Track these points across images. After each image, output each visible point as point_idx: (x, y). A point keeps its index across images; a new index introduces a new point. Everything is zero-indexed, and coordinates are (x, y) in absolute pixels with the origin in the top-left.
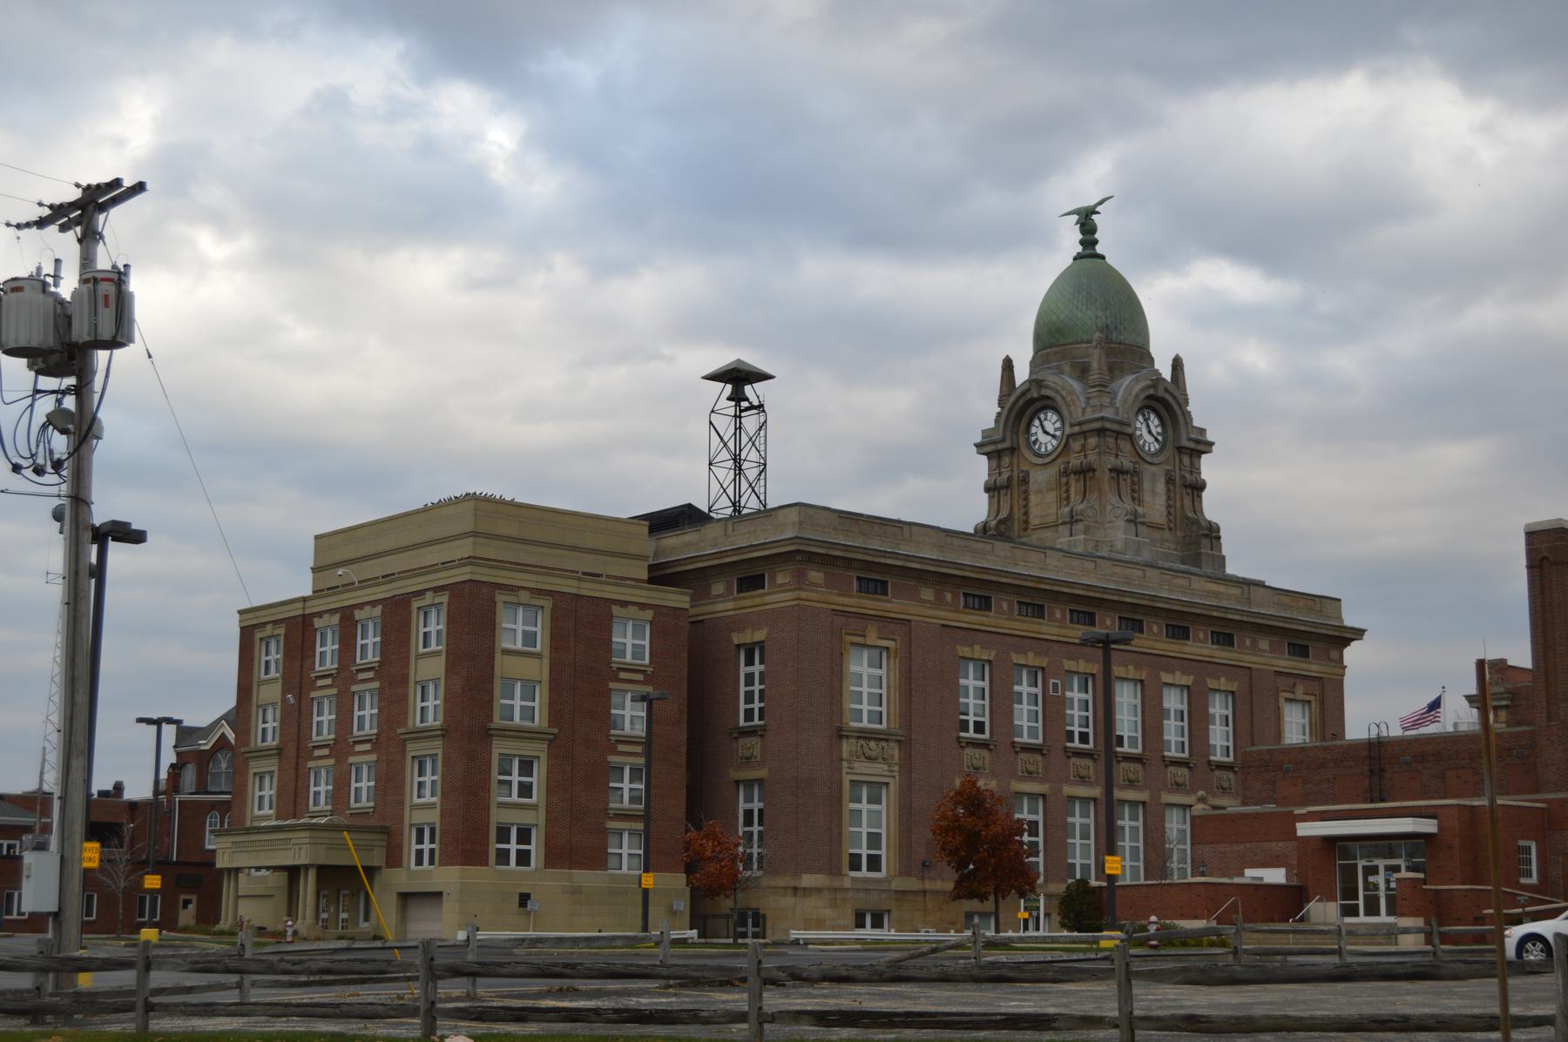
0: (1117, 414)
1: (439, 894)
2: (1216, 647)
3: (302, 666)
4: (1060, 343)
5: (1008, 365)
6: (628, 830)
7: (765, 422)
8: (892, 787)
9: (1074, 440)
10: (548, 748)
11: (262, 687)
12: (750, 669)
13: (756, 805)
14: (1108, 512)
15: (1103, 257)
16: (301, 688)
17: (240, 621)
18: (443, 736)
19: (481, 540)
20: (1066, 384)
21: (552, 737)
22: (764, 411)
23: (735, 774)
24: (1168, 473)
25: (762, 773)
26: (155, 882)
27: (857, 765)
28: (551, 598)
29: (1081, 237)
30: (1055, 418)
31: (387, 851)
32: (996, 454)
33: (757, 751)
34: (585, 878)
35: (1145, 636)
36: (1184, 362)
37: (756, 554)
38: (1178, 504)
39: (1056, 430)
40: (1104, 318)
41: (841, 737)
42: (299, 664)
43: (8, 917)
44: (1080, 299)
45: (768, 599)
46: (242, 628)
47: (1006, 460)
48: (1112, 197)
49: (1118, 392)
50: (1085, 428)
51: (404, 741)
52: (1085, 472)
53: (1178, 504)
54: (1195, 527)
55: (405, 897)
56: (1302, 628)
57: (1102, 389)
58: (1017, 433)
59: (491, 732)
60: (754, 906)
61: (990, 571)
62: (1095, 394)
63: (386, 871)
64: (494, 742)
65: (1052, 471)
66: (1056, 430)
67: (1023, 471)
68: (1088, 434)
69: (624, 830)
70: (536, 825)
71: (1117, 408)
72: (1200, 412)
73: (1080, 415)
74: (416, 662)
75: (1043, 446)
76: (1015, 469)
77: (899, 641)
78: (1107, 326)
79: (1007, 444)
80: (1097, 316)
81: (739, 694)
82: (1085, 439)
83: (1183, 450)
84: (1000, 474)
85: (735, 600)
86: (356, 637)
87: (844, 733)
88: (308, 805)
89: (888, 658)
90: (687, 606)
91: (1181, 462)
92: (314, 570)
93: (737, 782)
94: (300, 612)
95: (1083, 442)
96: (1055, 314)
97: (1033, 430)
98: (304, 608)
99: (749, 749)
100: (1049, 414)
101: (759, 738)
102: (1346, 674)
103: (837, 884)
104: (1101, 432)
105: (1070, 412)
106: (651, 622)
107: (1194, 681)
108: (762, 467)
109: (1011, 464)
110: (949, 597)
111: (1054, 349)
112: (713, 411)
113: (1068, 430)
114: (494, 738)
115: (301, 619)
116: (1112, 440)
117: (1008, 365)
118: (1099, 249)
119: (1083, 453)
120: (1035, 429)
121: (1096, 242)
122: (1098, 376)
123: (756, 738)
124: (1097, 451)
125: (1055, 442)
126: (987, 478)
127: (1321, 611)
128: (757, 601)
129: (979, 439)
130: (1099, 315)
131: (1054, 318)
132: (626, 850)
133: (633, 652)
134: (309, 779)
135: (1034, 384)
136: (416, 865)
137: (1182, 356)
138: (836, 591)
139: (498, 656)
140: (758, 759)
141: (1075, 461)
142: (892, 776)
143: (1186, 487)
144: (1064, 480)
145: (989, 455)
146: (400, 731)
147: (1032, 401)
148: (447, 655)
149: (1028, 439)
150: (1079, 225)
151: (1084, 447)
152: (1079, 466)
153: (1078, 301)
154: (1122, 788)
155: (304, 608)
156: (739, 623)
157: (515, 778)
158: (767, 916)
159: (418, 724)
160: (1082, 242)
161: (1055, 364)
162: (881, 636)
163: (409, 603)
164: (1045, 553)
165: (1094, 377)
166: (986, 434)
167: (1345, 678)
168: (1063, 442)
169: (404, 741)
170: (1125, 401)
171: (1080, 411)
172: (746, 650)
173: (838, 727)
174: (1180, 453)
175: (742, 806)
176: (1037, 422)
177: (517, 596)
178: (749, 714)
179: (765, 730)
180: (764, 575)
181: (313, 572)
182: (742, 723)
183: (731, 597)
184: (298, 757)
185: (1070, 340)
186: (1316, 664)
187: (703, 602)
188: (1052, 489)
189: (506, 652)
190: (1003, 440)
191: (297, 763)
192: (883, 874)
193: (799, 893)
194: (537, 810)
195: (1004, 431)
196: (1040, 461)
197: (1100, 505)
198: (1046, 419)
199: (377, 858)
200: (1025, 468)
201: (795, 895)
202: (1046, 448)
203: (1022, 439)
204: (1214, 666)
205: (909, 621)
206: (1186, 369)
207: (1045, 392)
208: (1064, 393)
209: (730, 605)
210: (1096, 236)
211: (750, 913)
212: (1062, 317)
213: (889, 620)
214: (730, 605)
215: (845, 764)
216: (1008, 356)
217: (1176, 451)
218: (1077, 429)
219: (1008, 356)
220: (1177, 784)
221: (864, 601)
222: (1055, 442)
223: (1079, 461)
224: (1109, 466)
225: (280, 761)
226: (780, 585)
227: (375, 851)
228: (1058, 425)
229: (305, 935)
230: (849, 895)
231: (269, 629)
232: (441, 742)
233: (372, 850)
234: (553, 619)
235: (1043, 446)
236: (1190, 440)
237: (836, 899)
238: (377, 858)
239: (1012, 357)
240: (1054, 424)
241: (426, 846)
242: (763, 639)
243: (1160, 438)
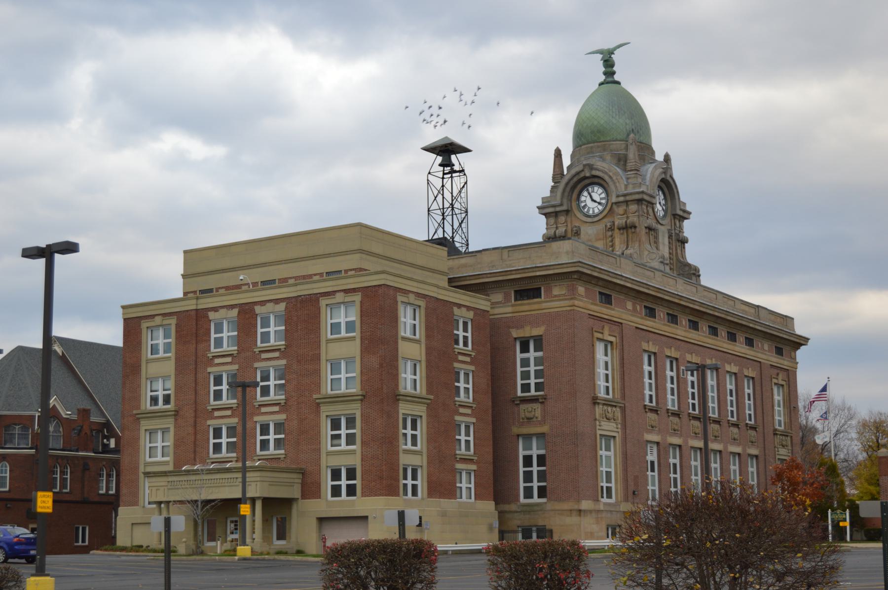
0: (648, 189)
1: (365, 518)
2: (748, 347)
3: (196, 349)
4: (601, 140)
5: (558, 154)
6: (466, 470)
7: (466, 183)
8: (617, 438)
9: (618, 206)
10: (427, 410)
11: (149, 365)
12: (525, 355)
13: (535, 452)
14: (645, 256)
15: (618, 83)
16: (196, 364)
17: (123, 314)
18: (361, 400)
19: (364, 256)
20: (605, 165)
21: (429, 401)
22: (465, 174)
23: (516, 430)
24: (669, 231)
25: (544, 429)
26: (246, 510)
27: (603, 423)
28: (424, 300)
29: (604, 69)
30: (600, 190)
31: (302, 487)
32: (554, 214)
33: (538, 413)
34: (446, 504)
35: (719, 338)
36: (672, 157)
37: (538, 274)
38: (674, 253)
39: (601, 199)
40: (630, 124)
41: (595, 403)
42: (194, 346)
43: (76, 544)
44: (614, 111)
45: (544, 305)
46: (125, 319)
47: (562, 219)
48: (629, 43)
49: (646, 175)
50: (628, 198)
51: (318, 404)
52: (628, 228)
53: (674, 253)
54: (687, 269)
55: (321, 520)
56: (785, 336)
57: (636, 172)
58: (571, 201)
59: (398, 397)
60: (541, 523)
61: (661, 291)
62: (633, 176)
63: (301, 502)
64: (400, 405)
65: (601, 227)
66: (601, 199)
67: (576, 227)
68: (629, 203)
69: (463, 470)
70: (421, 466)
71: (648, 186)
72: (685, 194)
73: (623, 190)
74: (326, 346)
75: (591, 209)
76: (569, 225)
77: (618, 338)
78: (633, 130)
79: (564, 208)
80: (626, 124)
81: (516, 373)
82: (627, 205)
83: (676, 217)
84: (557, 228)
85: (513, 306)
86: (257, 327)
87: (598, 401)
88: (208, 453)
89: (612, 349)
90: (488, 309)
91: (675, 224)
92: (184, 276)
93: (518, 436)
94: (194, 307)
95: (625, 208)
96: (596, 120)
97: (583, 199)
98: (197, 304)
99: (531, 411)
100: (596, 188)
101: (539, 404)
102: (798, 367)
103: (597, 508)
104: (639, 201)
105: (616, 187)
106: (472, 320)
107: (739, 370)
108: (463, 215)
109: (566, 221)
110: (638, 307)
111: (596, 144)
112: (429, 173)
113: (614, 199)
114: (400, 402)
115: (193, 313)
116: (645, 207)
117: (558, 154)
118: (616, 77)
119: (625, 216)
120: (585, 197)
121: (614, 73)
122: (634, 163)
123: (537, 404)
124: (637, 214)
125: (601, 208)
126: (545, 231)
127: (787, 325)
128: (536, 307)
129: (540, 204)
130: (628, 122)
131: (595, 123)
132: (466, 484)
133: (464, 341)
134: (209, 434)
135: (587, 167)
136: (332, 496)
137: (670, 153)
138: (591, 301)
139: (400, 341)
140: (539, 419)
141: (619, 221)
142: (617, 432)
143: (679, 241)
144: (610, 233)
145: (547, 215)
146: (315, 396)
147: (585, 178)
148: (361, 339)
149: (579, 205)
150: (602, 61)
151: (625, 212)
152: (624, 224)
153: (613, 112)
154: (712, 442)
155: (197, 304)
156: (519, 323)
157: (409, 432)
158: (554, 531)
159: (329, 392)
160: (605, 73)
161: (598, 154)
162: (612, 334)
163: (318, 301)
164: (676, 280)
165: (631, 164)
166: (545, 201)
167: (798, 370)
168: (608, 208)
169: (318, 404)
170: (651, 181)
171: (623, 187)
172: (535, 341)
173: (593, 397)
174: (675, 218)
175: (522, 453)
176: (585, 193)
177: (408, 297)
178: (526, 388)
179: (545, 399)
180: (540, 288)
181: (183, 278)
182: (519, 394)
183: (510, 304)
184: (196, 417)
185: (608, 139)
186: (788, 361)
187: (498, 306)
188: (600, 239)
189: (404, 339)
190: (561, 205)
191: (195, 422)
192: (613, 500)
193: (582, 513)
194: (422, 455)
195: (562, 198)
196: (589, 220)
197: (640, 251)
198: (593, 192)
199: (296, 493)
200: (577, 225)
201: (580, 515)
202: (594, 211)
203: (574, 204)
204: (745, 360)
205: (621, 323)
206: (672, 162)
207: (594, 173)
208: (611, 174)
209: (509, 309)
210: (615, 69)
211: (534, 529)
212: (602, 122)
213: (613, 323)
214: (509, 309)
215: (598, 423)
216: (558, 148)
217: (672, 217)
218: (621, 199)
219: (558, 148)
220: (734, 439)
221: (603, 309)
222: (601, 208)
223: (624, 221)
224: (646, 225)
225: (176, 420)
226: (556, 296)
227: (295, 487)
228: (603, 195)
229: (260, 551)
230: (604, 515)
231: (158, 320)
232: (359, 405)
233: (293, 486)
234: (427, 316)
235: (591, 209)
236: (681, 210)
237: (598, 518)
238: (296, 493)
239: (560, 148)
240: (599, 195)
241: (410, 482)
242: (541, 334)
243: (664, 207)
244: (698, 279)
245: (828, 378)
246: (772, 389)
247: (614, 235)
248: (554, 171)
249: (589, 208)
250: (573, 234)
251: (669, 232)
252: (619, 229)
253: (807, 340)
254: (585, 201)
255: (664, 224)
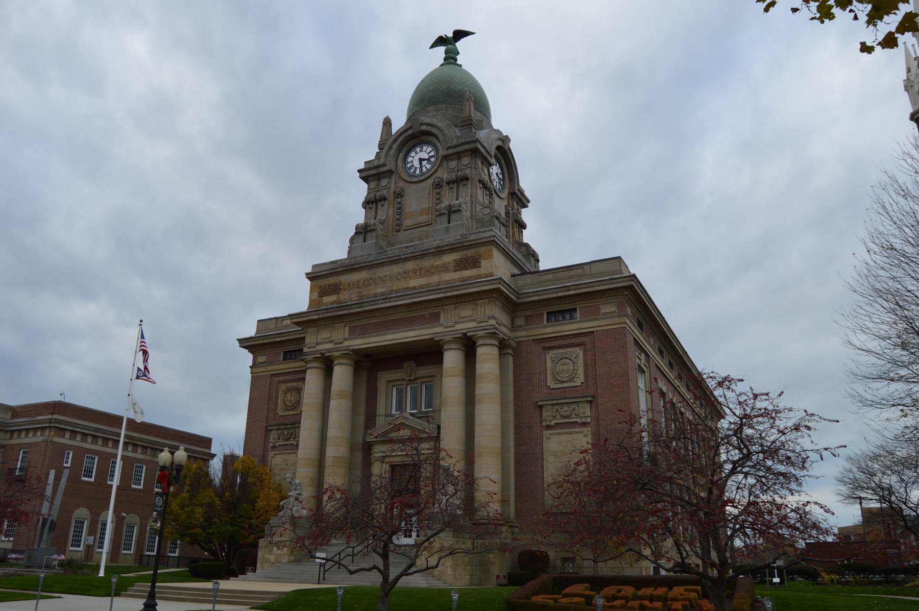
15: (460, 66)
129: (362, 166)
174: (512, 198)
240: (428, 153)
244: (537, 265)
245: (141, 321)
246: (637, 377)
247: (441, 198)
248: (381, 138)
249: (413, 165)
250: (396, 195)
251: (506, 208)
252: (448, 183)
253: (216, 455)
254: (412, 162)
255: (503, 197)
